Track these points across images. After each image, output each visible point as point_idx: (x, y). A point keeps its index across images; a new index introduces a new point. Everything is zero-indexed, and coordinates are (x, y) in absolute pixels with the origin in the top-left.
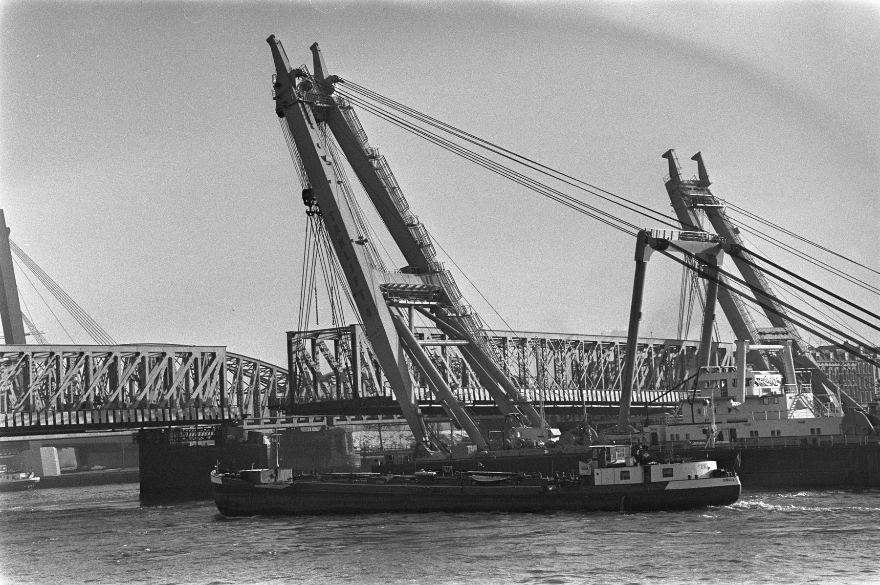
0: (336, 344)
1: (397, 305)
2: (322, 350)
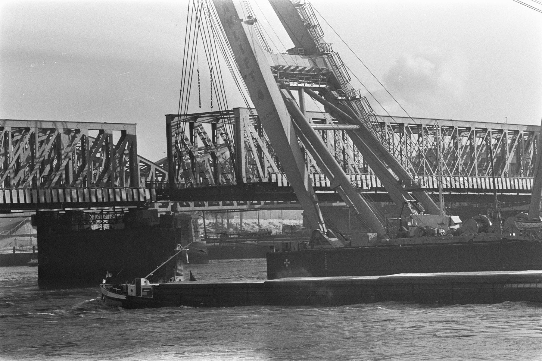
0: (214, 127)
1: (290, 88)
2: (199, 133)
